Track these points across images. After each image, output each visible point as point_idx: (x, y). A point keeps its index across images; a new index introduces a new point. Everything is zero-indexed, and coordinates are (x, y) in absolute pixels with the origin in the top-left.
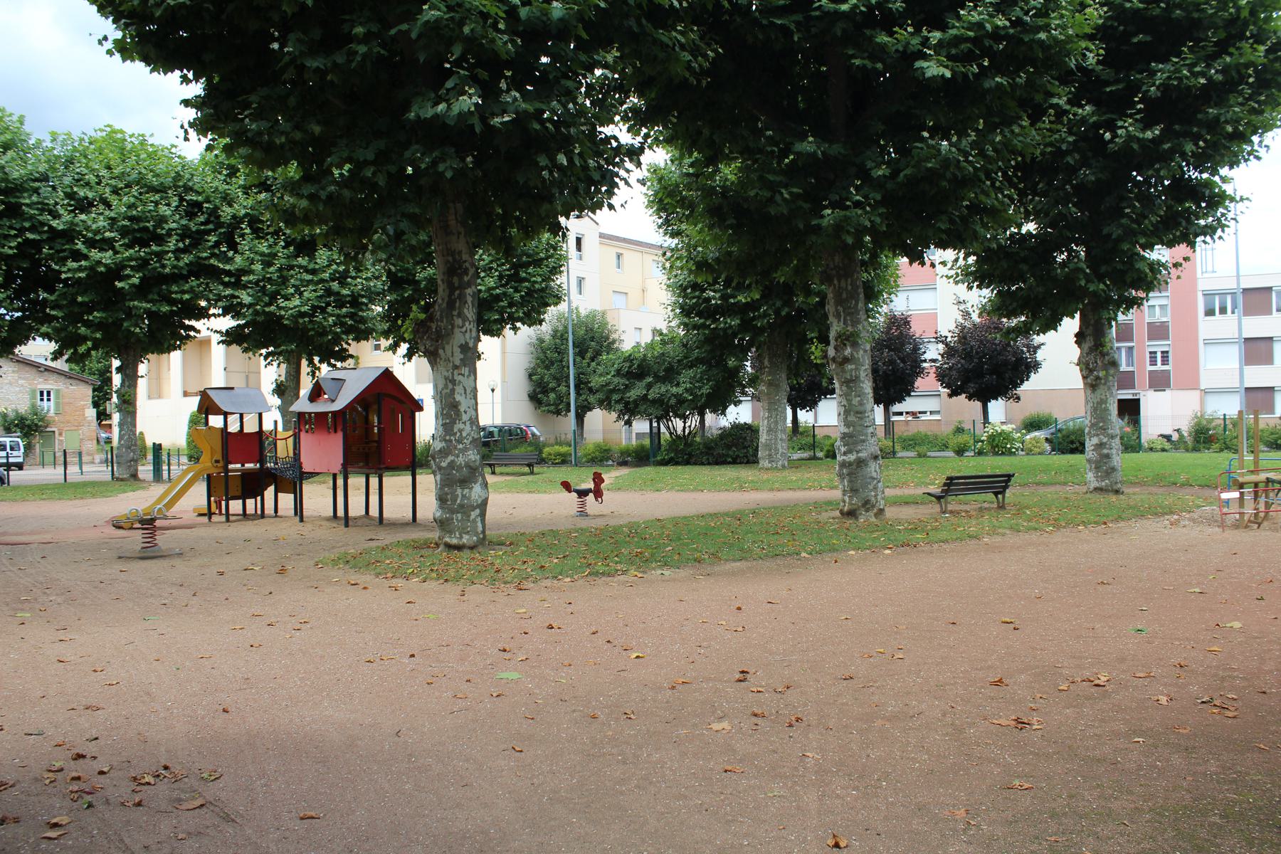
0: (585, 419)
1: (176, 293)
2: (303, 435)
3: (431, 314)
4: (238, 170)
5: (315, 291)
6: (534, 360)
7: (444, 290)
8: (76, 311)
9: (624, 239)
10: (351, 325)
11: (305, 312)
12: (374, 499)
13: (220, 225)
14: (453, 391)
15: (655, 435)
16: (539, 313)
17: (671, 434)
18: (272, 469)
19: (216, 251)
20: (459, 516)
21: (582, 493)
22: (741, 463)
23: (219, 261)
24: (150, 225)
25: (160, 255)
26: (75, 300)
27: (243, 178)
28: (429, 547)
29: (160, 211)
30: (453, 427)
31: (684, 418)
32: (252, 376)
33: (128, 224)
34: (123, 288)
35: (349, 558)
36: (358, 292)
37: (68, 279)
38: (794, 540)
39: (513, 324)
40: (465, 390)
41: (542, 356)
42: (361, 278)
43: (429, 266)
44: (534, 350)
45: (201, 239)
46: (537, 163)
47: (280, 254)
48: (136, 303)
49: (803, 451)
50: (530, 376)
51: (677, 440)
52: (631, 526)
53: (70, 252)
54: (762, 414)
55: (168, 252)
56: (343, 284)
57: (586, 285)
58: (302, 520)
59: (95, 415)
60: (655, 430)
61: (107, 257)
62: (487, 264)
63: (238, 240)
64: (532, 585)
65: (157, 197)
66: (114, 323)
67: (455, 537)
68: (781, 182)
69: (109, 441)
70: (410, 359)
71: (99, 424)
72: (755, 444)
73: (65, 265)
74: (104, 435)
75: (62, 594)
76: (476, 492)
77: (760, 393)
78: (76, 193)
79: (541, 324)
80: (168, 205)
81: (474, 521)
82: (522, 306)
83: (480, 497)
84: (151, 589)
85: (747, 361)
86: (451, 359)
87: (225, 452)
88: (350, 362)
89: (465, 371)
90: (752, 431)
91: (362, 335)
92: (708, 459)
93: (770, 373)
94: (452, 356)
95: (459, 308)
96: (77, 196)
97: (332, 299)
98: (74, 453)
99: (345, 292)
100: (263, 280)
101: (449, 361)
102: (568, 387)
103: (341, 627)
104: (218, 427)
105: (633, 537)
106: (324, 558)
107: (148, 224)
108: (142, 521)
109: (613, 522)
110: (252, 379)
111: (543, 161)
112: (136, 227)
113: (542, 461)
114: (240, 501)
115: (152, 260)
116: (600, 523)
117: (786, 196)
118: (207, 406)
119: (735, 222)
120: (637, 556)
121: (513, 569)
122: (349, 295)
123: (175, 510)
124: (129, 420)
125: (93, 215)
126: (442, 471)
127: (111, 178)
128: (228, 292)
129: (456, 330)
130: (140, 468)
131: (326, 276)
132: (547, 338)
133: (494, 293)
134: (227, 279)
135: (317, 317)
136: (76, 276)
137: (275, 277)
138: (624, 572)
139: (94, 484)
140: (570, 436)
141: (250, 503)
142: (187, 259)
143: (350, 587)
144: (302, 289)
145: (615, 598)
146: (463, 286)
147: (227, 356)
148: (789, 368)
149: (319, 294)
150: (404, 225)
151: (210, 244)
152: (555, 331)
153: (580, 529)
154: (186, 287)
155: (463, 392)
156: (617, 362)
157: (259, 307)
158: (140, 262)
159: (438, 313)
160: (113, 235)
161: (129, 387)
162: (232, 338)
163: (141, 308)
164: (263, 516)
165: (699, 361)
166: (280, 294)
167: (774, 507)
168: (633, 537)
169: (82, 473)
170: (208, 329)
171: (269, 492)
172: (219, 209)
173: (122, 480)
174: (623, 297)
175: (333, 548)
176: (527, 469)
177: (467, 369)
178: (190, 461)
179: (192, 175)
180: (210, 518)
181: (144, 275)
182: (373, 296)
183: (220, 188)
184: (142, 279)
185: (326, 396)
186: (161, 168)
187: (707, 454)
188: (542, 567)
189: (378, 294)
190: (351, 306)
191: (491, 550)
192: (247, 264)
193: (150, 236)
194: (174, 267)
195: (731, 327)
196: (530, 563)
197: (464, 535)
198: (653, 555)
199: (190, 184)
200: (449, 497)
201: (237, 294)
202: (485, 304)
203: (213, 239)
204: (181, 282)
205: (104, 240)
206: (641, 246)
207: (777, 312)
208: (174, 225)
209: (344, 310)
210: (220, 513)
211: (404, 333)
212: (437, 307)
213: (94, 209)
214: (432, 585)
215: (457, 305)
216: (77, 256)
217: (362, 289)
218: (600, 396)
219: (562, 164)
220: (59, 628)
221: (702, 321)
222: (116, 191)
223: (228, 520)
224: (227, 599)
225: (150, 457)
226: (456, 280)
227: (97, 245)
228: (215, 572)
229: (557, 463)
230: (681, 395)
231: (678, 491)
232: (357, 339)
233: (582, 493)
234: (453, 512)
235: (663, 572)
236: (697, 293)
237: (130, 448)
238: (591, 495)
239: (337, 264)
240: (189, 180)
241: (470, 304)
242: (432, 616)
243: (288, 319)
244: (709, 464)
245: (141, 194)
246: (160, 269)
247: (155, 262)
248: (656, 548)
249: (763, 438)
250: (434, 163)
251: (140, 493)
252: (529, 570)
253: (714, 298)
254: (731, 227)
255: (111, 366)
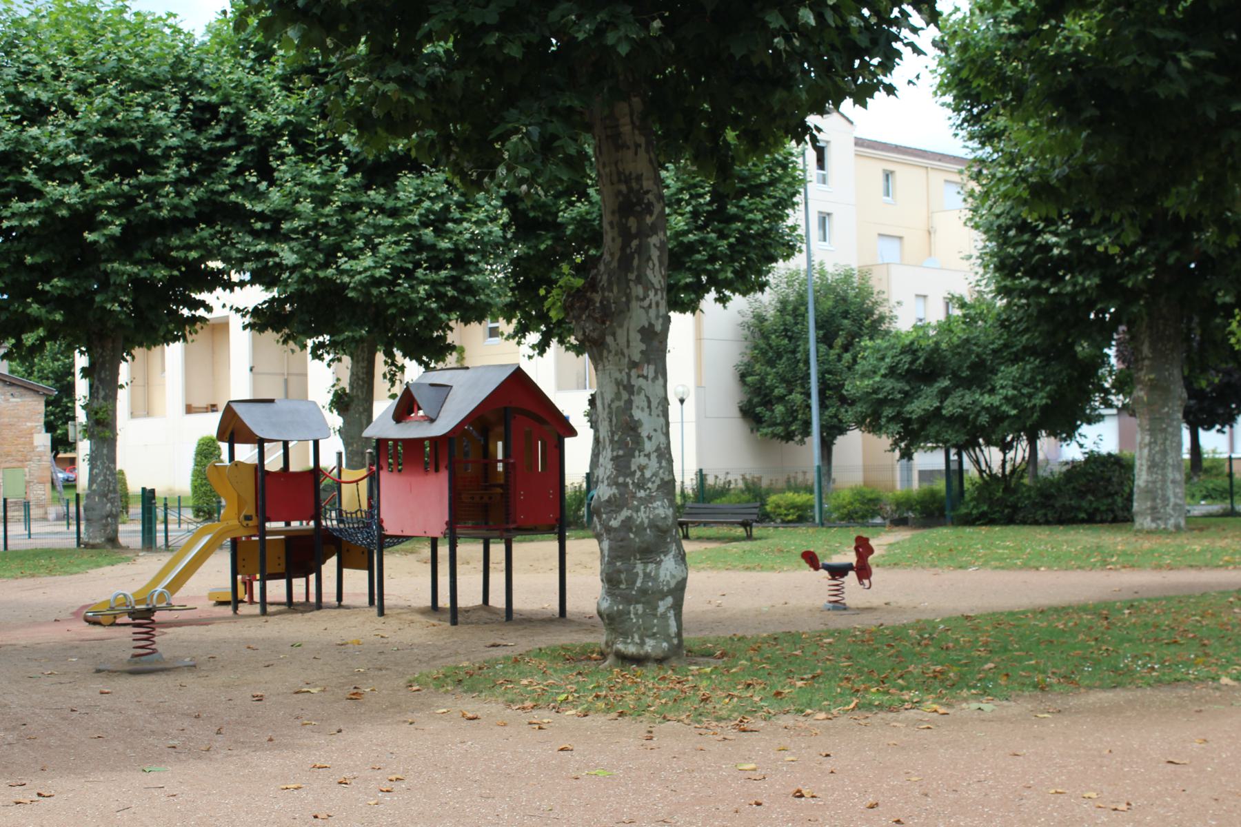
0: (835, 448)
1: (178, 248)
2: (384, 476)
3: (594, 279)
4: (273, 52)
5: (397, 243)
6: (748, 351)
7: (613, 240)
8: (22, 279)
9: (897, 147)
10: (453, 297)
11: (381, 277)
12: (497, 580)
13: (244, 140)
14: (629, 403)
15: (954, 474)
16: (760, 273)
17: (981, 471)
18: (334, 530)
19: (240, 181)
20: (640, 607)
21: (837, 572)
22: (1102, 521)
23: (245, 197)
24: (137, 141)
25: (152, 189)
26: (21, 261)
27: (281, 64)
28: (589, 658)
29: (152, 120)
30: (629, 462)
31: (1005, 447)
32: (293, 381)
33: (103, 140)
34: (96, 242)
35: (461, 675)
36: (464, 244)
37: (11, 229)
38: (1207, 655)
39: (718, 292)
40: (649, 402)
41: (762, 344)
42: (469, 221)
43: (579, 200)
44: (749, 333)
45: (216, 162)
46: (764, 25)
47: (339, 187)
48: (116, 265)
49: (1209, 501)
50: (743, 377)
51: (990, 481)
52: (921, 626)
53: (15, 187)
54: (1138, 438)
55: (165, 184)
56: (440, 232)
57: (834, 225)
58: (381, 612)
59: (49, 443)
60: (954, 466)
61: (71, 194)
62: (672, 195)
63: (274, 164)
64: (763, 724)
65: (147, 97)
66: (81, 297)
67: (633, 642)
68: (1176, 40)
69: (70, 484)
70: (542, 352)
71: (55, 457)
72: (1127, 490)
73: (6, 207)
74: (61, 475)
75: (14, 728)
76: (667, 568)
77: (1136, 401)
78: (22, 94)
79: (762, 290)
80: (165, 109)
81: (664, 616)
82: (732, 259)
83: (673, 576)
84: (150, 723)
85: (1109, 346)
86: (626, 351)
87: (260, 503)
88: (451, 359)
89: (649, 370)
90: (1122, 466)
91: (474, 313)
92: (1045, 515)
93: (1151, 369)
94: (628, 346)
95: (639, 267)
96: (24, 98)
97: (424, 255)
98: (16, 503)
99: (445, 244)
100: (314, 227)
101: (623, 354)
102: (809, 395)
103: (455, 788)
104: (249, 462)
105: (926, 645)
106: (421, 675)
107: (133, 141)
108: (133, 614)
109: (890, 620)
110: (295, 382)
111: (775, 20)
112: (116, 145)
113: (765, 518)
114: (283, 582)
115: (141, 196)
116: (869, 621)
117: (1186, 64)
118: (233, 430)
119: (1097, 113)
120: (935, 677)
121: (731, 697)
122: (449, 250)
123: (178, 598)
124: (105, 451)
125: (50, 128)
126: (612, 535)
127: (76, 69)
128: (262, 246)
129: (634, 304)
130: (121, 528)
131: (414, 218)
132: (771, 313)
133: (685, 240)
134: (258, 225)
135: (400, 285)
136: (25, 224)
137: (333, 221)
138: (916, 705)
139: (50, 553)
140: (812, 477)
141: (299, 584)
142: (194, 194)
143: (465, 723)
144: (377, 241)
145: (904, 749)
146: (644, 233)
147: (255, 348)
148: (1189, 360)
149: (403, 248)
150: (556, 126)
151: (230, 170)
152: (784, 303)
153: (835, 631)
154: (193, 240)
155: (646, 404)
156: (890, 353)
157: (308, 271)
158: (122, 200)
159: (605, 277)
160: (80, 158)
161: (105, 399)
162: (262, 319)
163: (123, 273)
164: (319, 605)
165: (1030, 351)
166: (341, 250)
167: (1165, 598)
168: (926, 645)
169: (30, 535)
170: (224, 306)
171: (330, 567)
172: (244, 114)
173: (93, 547)
174: (896, 243)
175: (434, 658)
176: (740, 531)
177: (652, 368)
178: (197, 516)
179: (202, 61)
180: (235, 609)
181: (129, 221)
182: (487, 249)
183: (245, 81)
184: (125, 228)
185: (421, 413)
186: (151, 50)
187: (1044, 506)
188: (778, 694)
189: (497, 245)
190: (453, 268)
191: (691, 664)
192: (290, 202)
193: (136, 159)
194: (175, 207)
195: (1084, 290)
196: (758, 687)
197: (647, 640)
198: (962, 676)
199: (198, 75)
200: (623, 576)
201: (274, 249)
202: (678, 257)
203: (234, 161)
204: (186, 231)
205: (66, 167)
206: (923, 157)
207: (1161, 264)
208: (174, 141)
209: (443, 273)
210: (251, 601)
211: (549, 310)
212: (602, 268)
213: (51, 118)
214: (598, 721)
215: (636, 262)
216: (27, 193)
217: (470, 240)
218: (860, 408)
219: (806, 24)
220: (14, 784)
221: (1034, 283)
222: (83, 89)
223: (264, 612)
224: (271, 740)
225: (136, 509)
226: (632, 223)
227: (56, 175)
228: (249, 695)
229: (790, 522)
230: (998, 408)
231: (997, 568)
232: (466, 320)
233: (837, 572)
234: (628, 600)
235: (982, 706)
236: (1026, 237)
237: (106, 496)
238: (852, 575)
239: (430, 198)
240: (196, 70)
241: (656, 262)
242: (602, 773)
243: (354, 289)
244: (1047, 523)
245: (121, 92)
246: (153, 212)
247: (146, 201)
248: (966, 665)
249: (1142, 478)
250: (599, 32)
251: (120, 569)
252: (756, 699)
253: (1056, 245)
254: (1089, 123)
255: (72, 365)
